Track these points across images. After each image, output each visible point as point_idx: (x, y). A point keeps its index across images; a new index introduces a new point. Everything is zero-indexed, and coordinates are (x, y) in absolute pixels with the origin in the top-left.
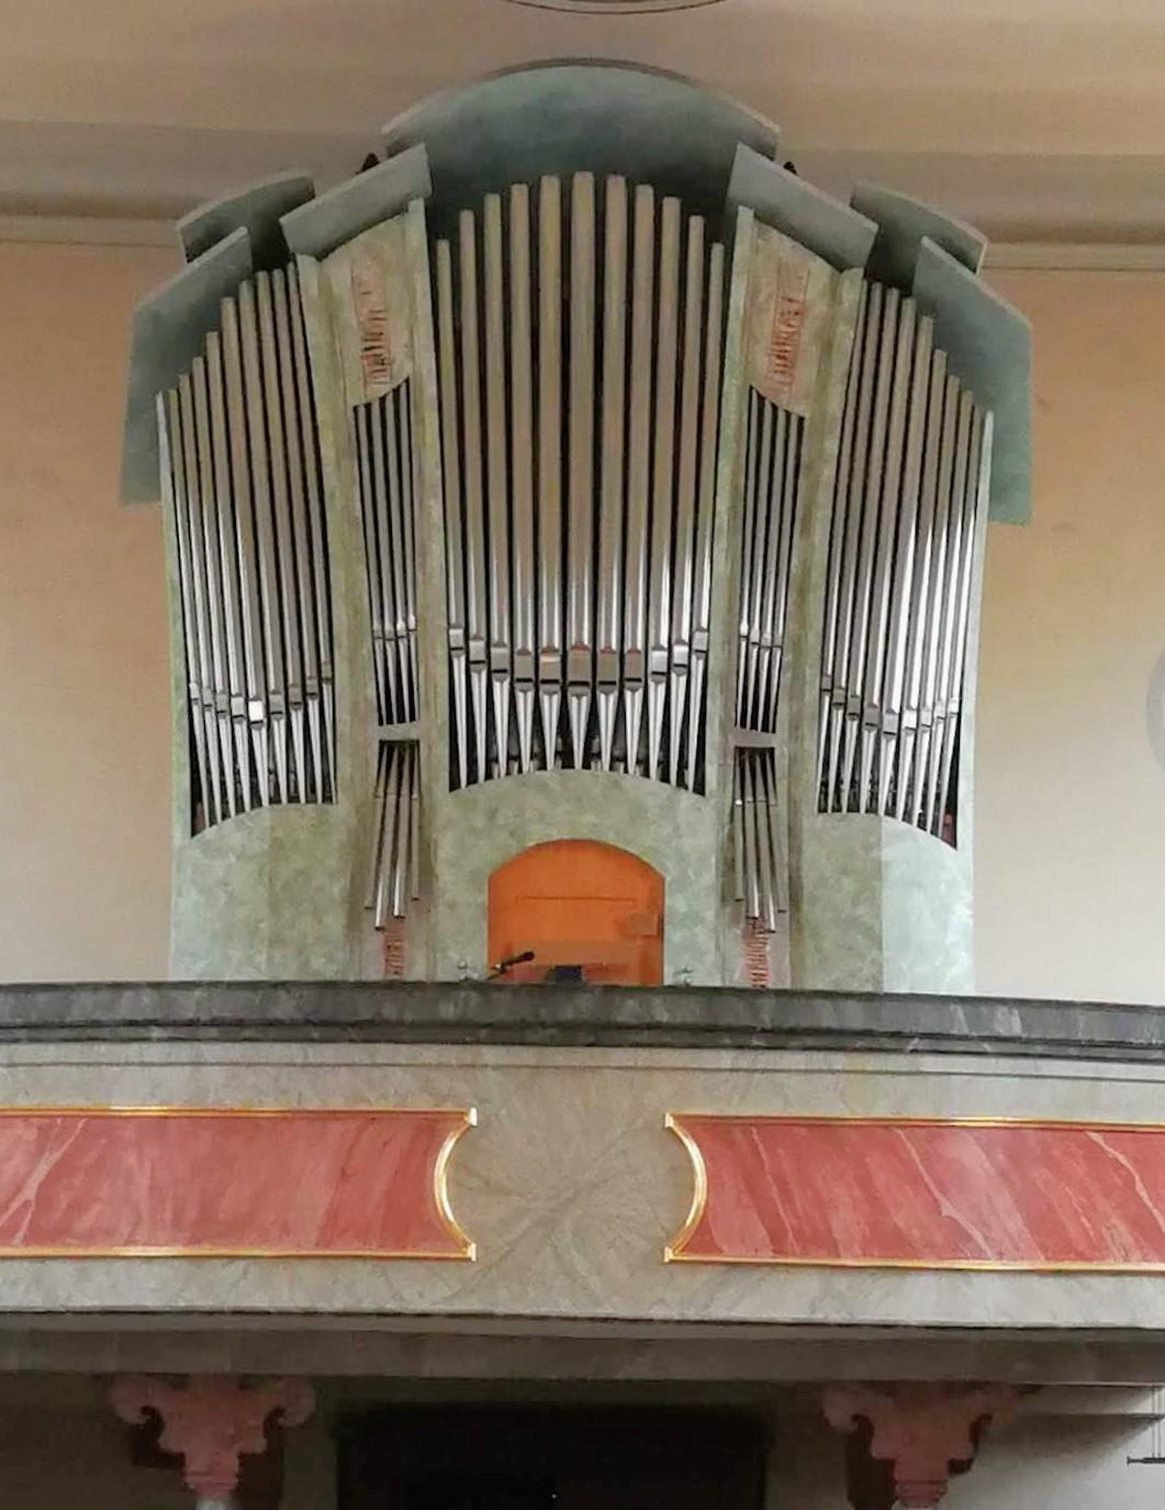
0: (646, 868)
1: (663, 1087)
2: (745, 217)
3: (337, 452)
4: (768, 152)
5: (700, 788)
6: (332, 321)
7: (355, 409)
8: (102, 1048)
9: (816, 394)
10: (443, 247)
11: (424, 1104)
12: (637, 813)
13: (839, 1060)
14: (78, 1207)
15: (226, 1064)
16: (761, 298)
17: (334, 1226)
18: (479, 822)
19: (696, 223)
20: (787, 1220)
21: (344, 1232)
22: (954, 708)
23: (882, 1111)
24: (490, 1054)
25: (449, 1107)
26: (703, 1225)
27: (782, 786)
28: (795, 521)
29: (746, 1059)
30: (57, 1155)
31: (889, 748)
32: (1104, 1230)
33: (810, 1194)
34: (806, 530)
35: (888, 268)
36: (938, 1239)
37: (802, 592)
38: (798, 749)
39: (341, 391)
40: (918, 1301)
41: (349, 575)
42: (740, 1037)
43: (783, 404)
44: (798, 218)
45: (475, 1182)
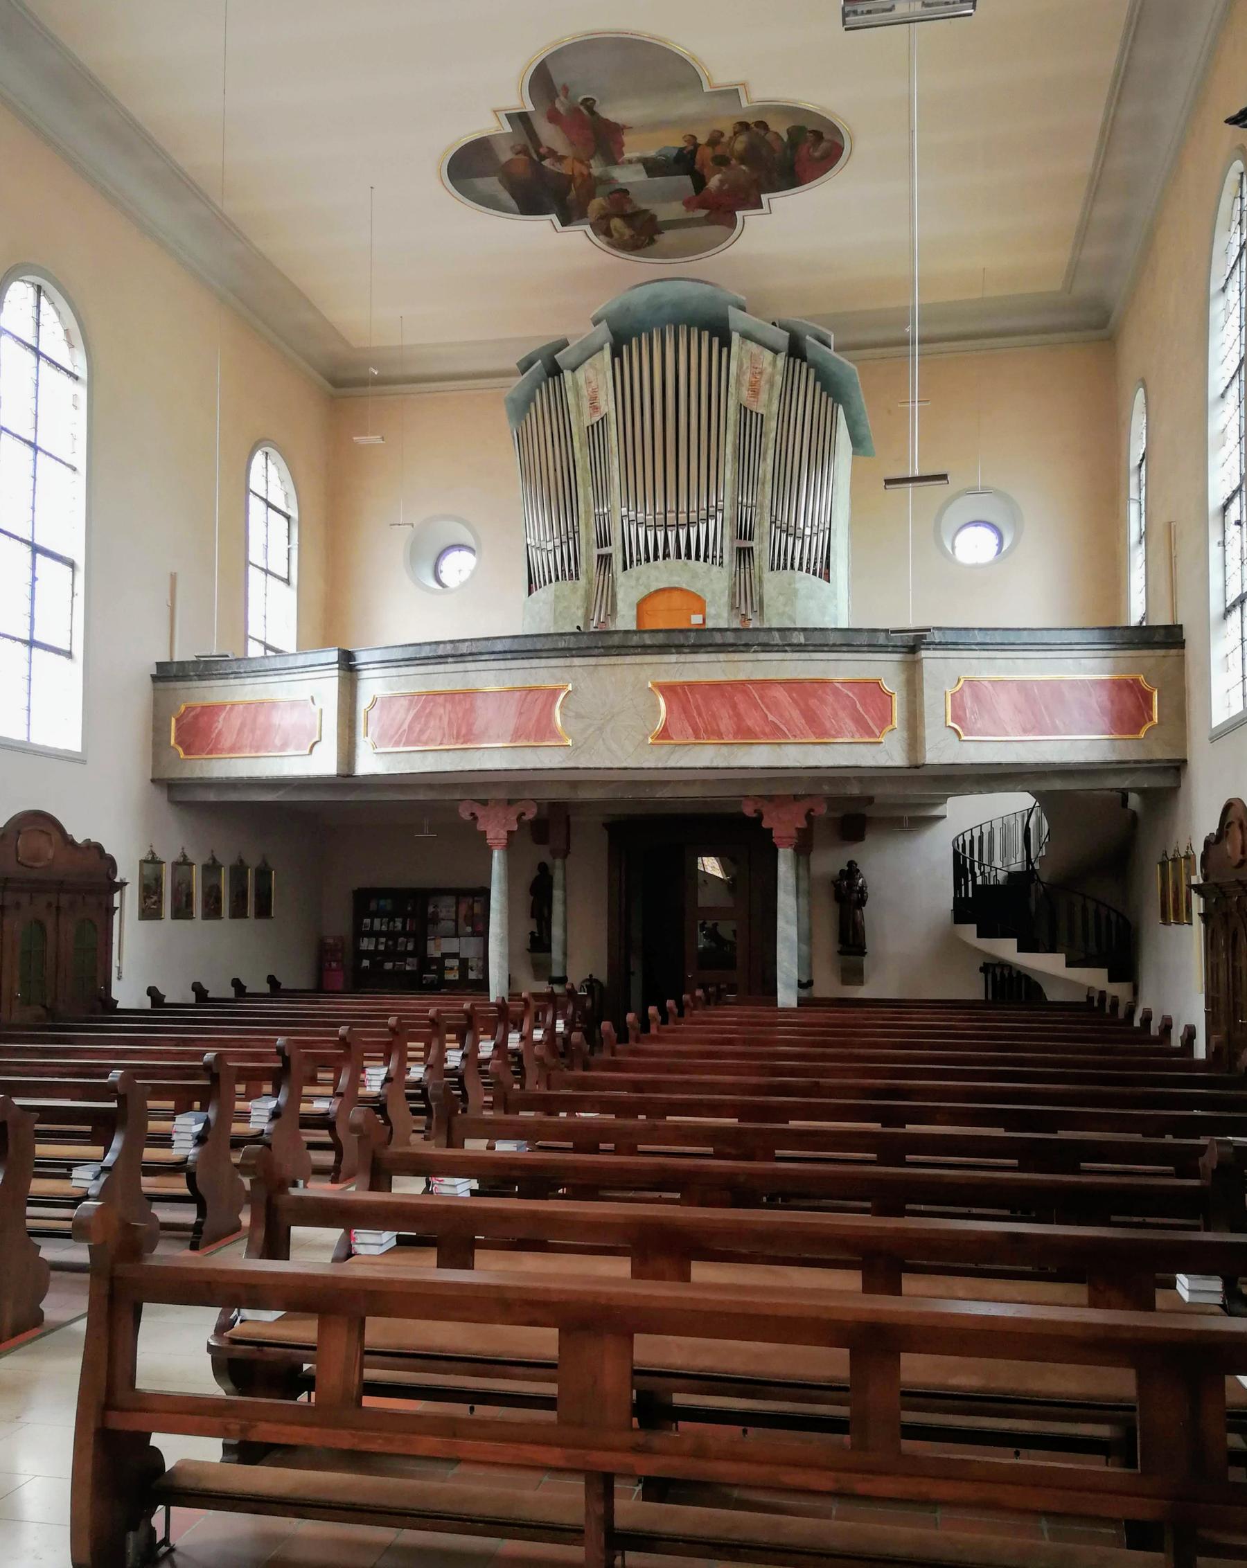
0: (699, 597)
1: (648, 671)
2: (735, 337)
4: (743, 309)
5: (721, 564)
6: (578, 396)
8: (431, 667)
9: (767, 405)
10: (617, 360)
12: (695, 576)
13: (722, 657)
14: (422, 731)
17: (517, 734)
18: (633, 583)
19: (716, 341)
22: (827, 525)
23: (741, 677)
24: (577, 661)
27: (756, 563)
29: (682, 658)
31: (799, 543)
34: (765, 459)
35: (796, 350)
36: (767, 730)
37: (763, 484)
38: (761, 547)
39: (581, 419)
40: (759, 756)
41: (585, 492)
42: (679, 648)
43: (754, 408)
44: (759, 335)
45: (571, 714)
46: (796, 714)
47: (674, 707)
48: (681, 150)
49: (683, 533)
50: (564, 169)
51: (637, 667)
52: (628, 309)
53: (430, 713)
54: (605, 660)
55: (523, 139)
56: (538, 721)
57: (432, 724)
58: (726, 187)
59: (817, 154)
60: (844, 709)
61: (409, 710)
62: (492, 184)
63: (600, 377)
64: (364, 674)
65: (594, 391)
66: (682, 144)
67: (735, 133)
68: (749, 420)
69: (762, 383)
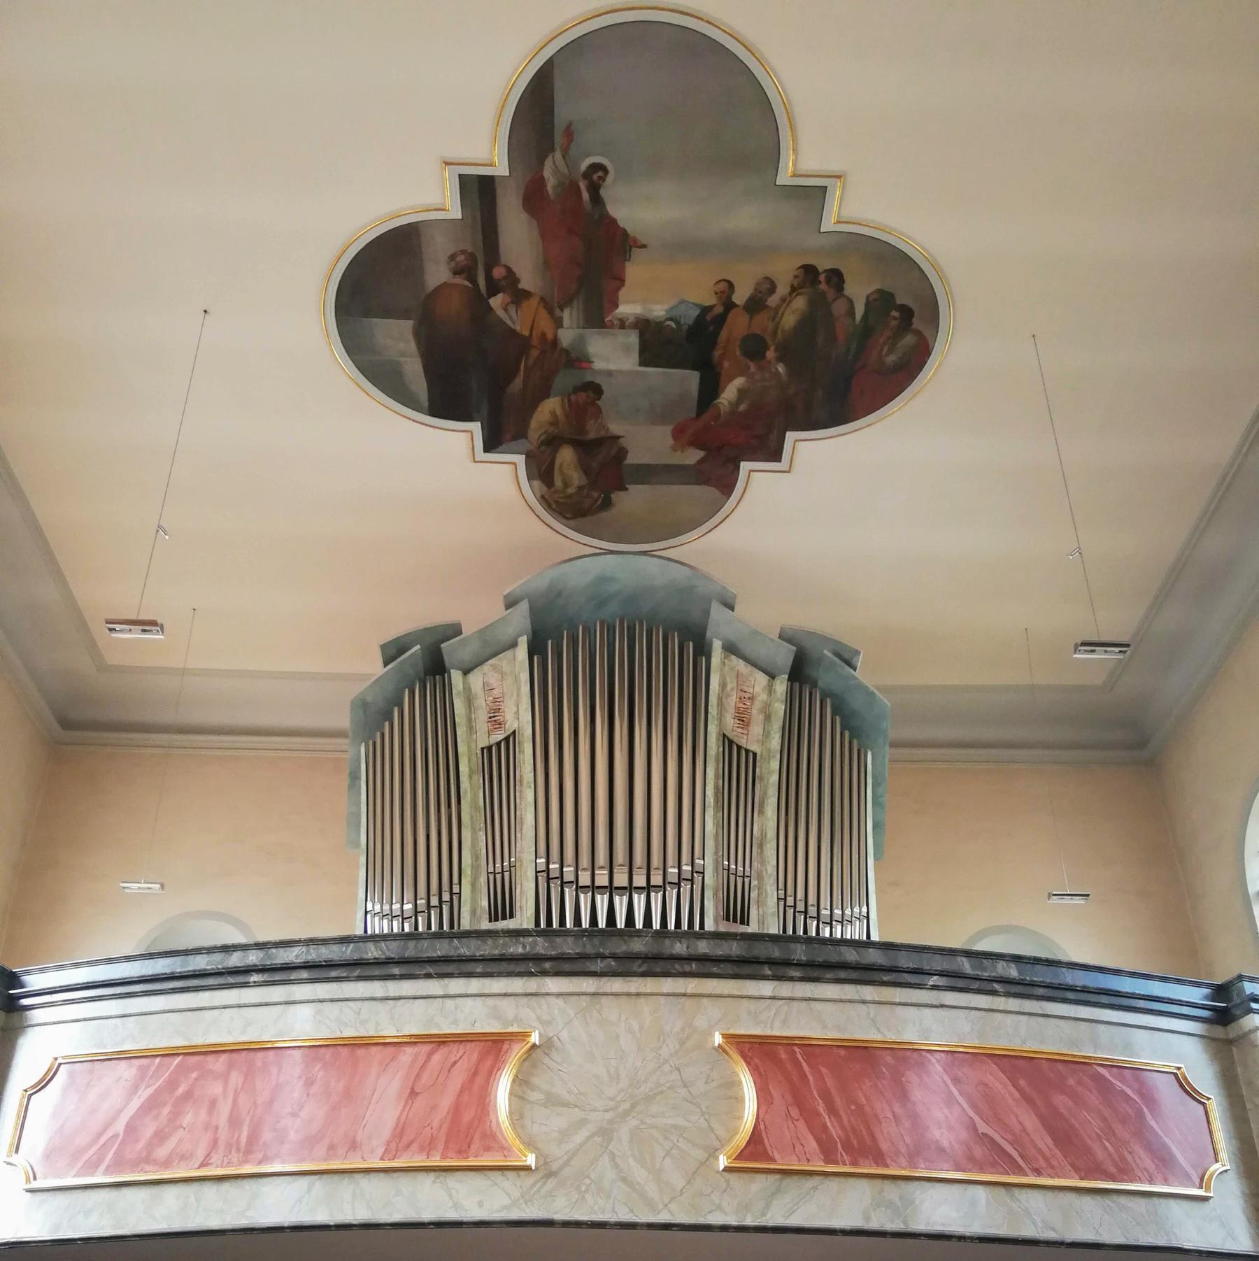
1: (712, 1010)
2: (717, 646)
3: (470, 769)
7: (483, 749)
11: (494, 1027)
13: (868, 992)
14: (160, 1137)
15: (313, 1001)
16: (729, 688)
17: (400, 1138)
20: (834, 1131)
21: (408, 1146)
24: (553, 984)
25: (514, 1029)
26: (756, 1138)
28: (753, 806)
29: (785, 989)
30: (150, 1091)
32: (1126, 1154)
33: (853, 1107)
34: (761, 812)
35: (800, 672)
37: (761, 846)
39: (473, 739)
46: (1030, 1122)
47: (776, 1093)
48: (706, 310)
49: (639, 901)
50: (518, 320)
51: (688, 1002)
52: (559, 594)
53: (188, 1095)
54: (617, 985)
55: (471, 243)
56: (456, 1110)
57: (187, 1119)
58: (742, 407)
59: (891, 359)
60: (1124, 1121)
61: (135, 1088)
62: (397, 338)
63: (509, 681)
64: (36, 1016)
65: (495, 700)
66: (709, 300)
67: (793, 289)
68: (739, 761)
69: (754, 712)
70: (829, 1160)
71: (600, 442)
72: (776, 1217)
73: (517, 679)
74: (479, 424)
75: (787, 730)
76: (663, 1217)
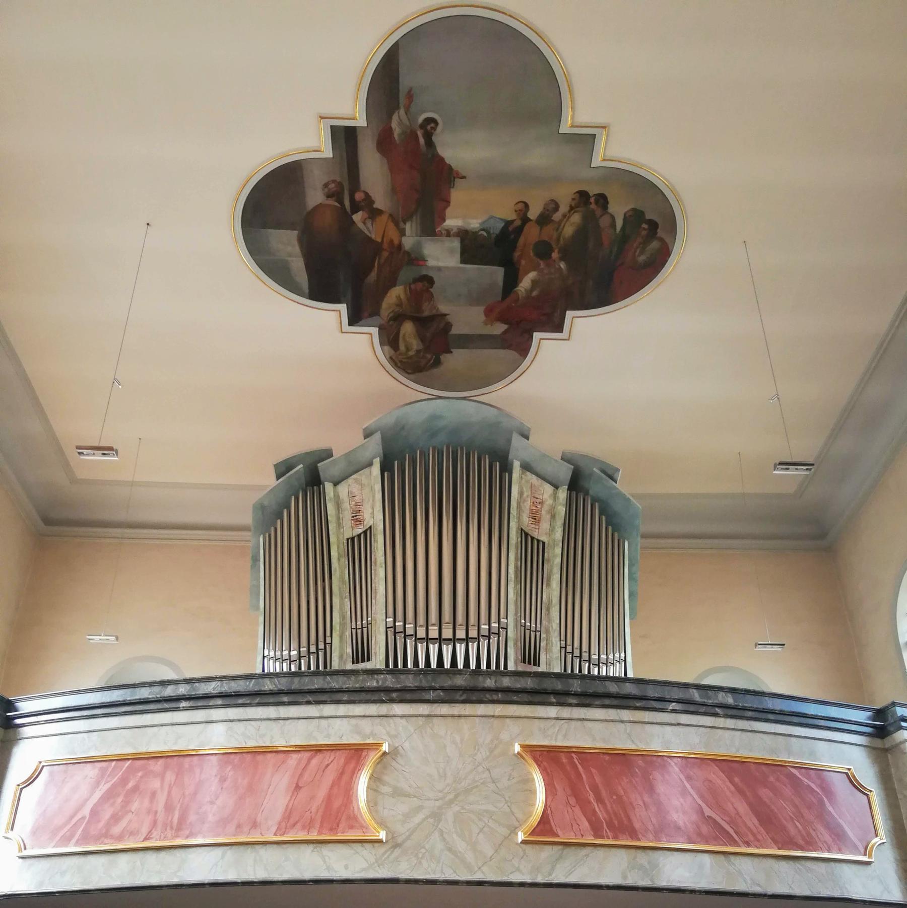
1: (513, 727)
2: (517, 465)
3: (339, 554)
7: (348, 539)
11: (356, 740)
13: (626, 714)
14: (115, 818)
15: (226, 721)
16: (525, 495)
17: (289, 820)
20: (601, 814)
21: (294, 825)
24: (398, 709)
25: (370, 741)
26: (544, 819)
28: (542, 580)
29: (566, 712)
30: (108, 785)
32: (811, 831)
33: (615, 797)
34: (548, 585)
35: (577, 484)
37: (548, 609)
39: (341, 532)
46: (742, 808)
47: (559, 787)
48: (508, 223)
50: (373, 230)
51: (496, 722)
52: (403, 428)
53: (136, 789)
54: (444, 709)
55: (339, 175)
56: (329, 799)
57: (135, 806)
58: (535, 293)
59: (642, 258)
60: (810, 807)
61: (97, 784)
62: (286, 243)
63: (367, 490)
64: (26, 731)
65: (357, 504)
66: (511, 216)
67: (572, 208)
68: (532, 548)
69: (543, 512)
70: (597, 835)
71: (432, 318)
72: (559, 877)
73: (372, 489)
74: (345, 305)
75: (567, 526)
76: (478, 877)
